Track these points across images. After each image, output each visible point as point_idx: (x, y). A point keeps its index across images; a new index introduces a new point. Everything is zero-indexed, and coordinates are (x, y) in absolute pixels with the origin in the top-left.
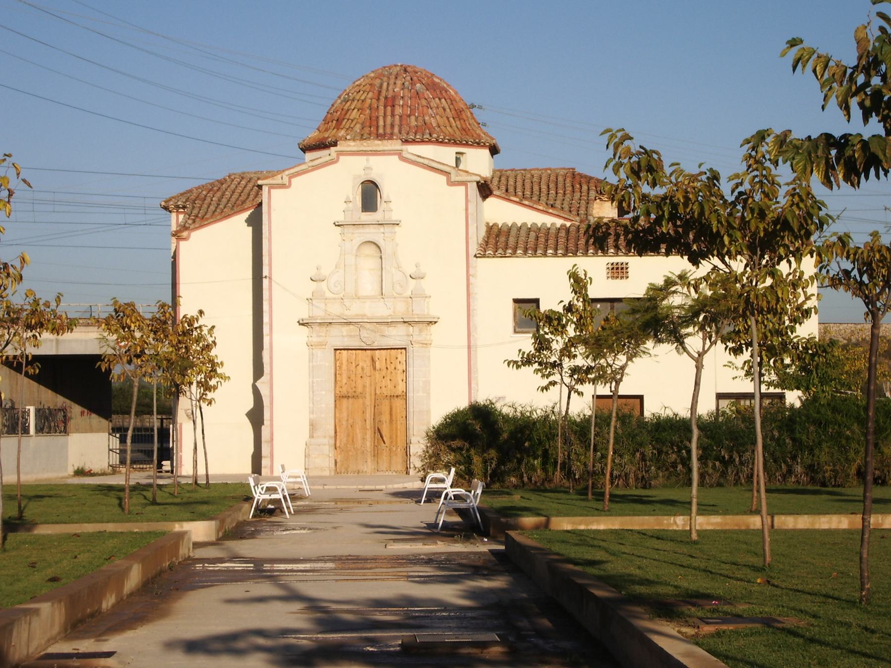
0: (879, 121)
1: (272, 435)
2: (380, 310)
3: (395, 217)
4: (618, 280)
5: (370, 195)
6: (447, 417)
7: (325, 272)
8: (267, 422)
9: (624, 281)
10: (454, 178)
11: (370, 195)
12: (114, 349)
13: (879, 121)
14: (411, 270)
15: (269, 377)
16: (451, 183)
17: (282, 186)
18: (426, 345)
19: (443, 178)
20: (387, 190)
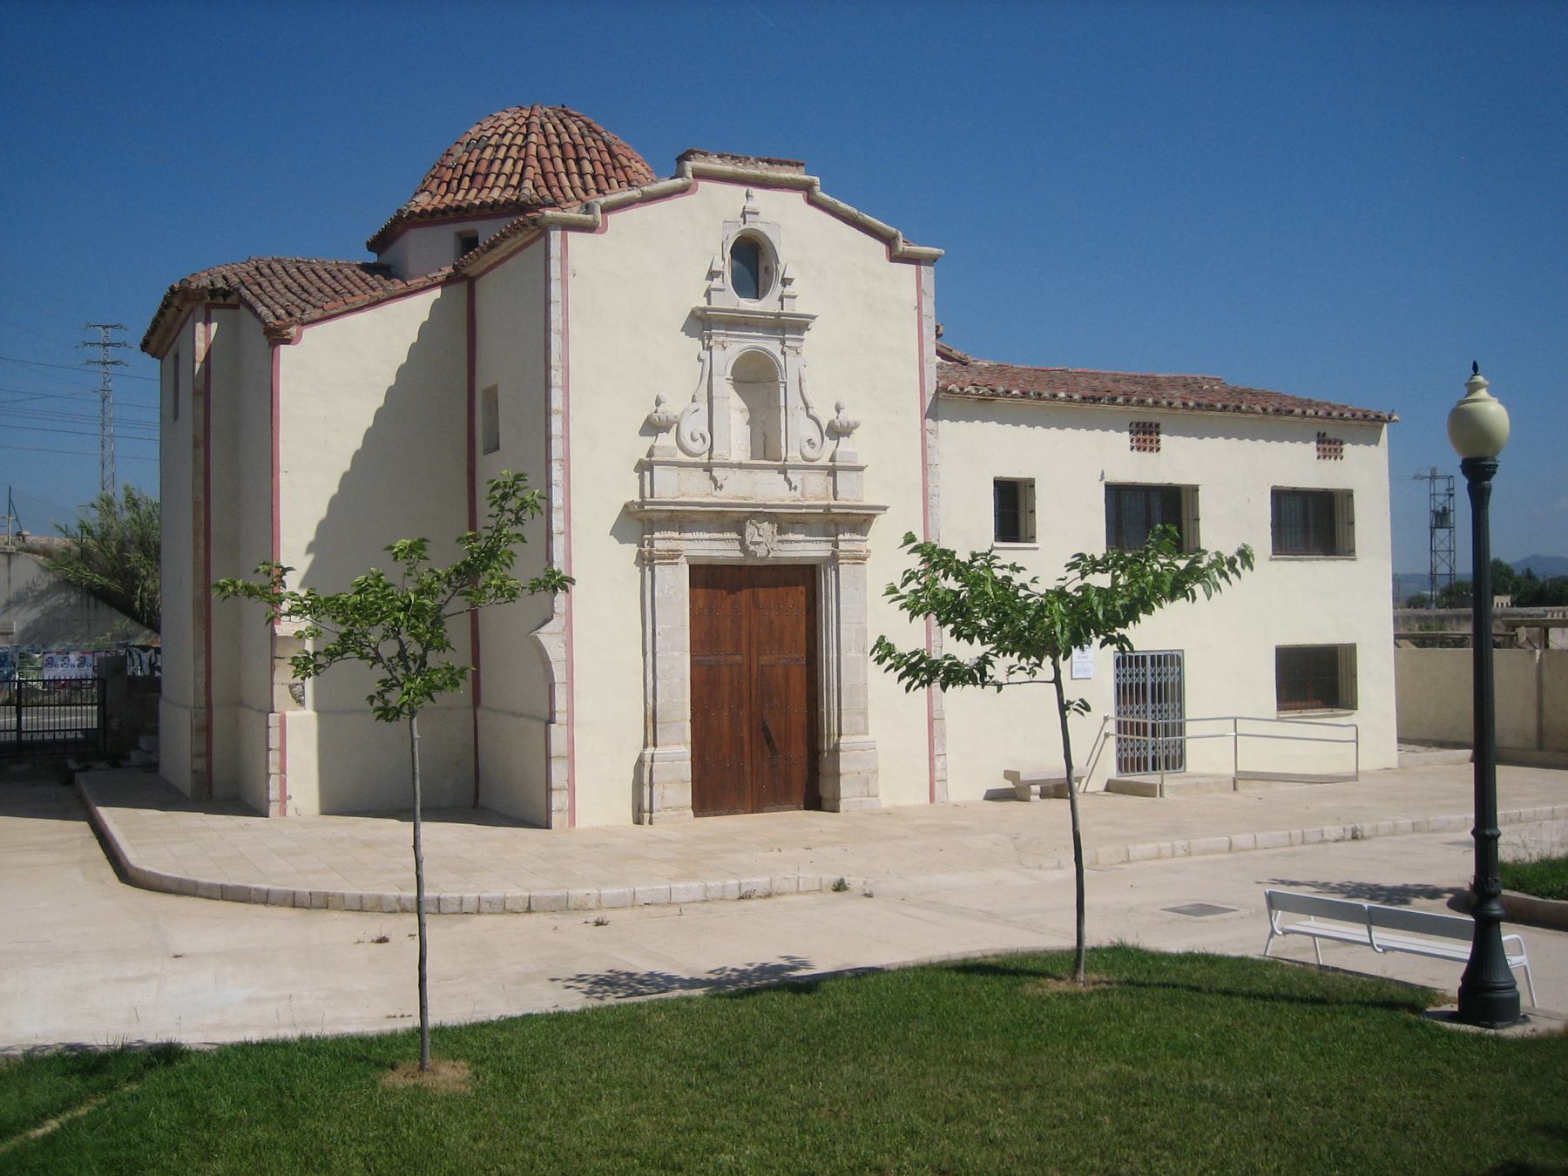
0: (1161, 606)
1: (571, 742)
2: (769, 489)
3: (797, 307)
4: (1147, 454)
5: (752, 260)
6: (71, 1047)
7: (671, 409)
8: (560, 717)
9: (1154, 455)
10: (901, 246)
11: (752, 260)
12: (476, 560)
13: (1161, 606)
14: (826, 416)
15: (563, 621)
16: (895, 257)
17: (589, 228)
18: (859, 559)
19: (880, 248)
20: (788, 256)
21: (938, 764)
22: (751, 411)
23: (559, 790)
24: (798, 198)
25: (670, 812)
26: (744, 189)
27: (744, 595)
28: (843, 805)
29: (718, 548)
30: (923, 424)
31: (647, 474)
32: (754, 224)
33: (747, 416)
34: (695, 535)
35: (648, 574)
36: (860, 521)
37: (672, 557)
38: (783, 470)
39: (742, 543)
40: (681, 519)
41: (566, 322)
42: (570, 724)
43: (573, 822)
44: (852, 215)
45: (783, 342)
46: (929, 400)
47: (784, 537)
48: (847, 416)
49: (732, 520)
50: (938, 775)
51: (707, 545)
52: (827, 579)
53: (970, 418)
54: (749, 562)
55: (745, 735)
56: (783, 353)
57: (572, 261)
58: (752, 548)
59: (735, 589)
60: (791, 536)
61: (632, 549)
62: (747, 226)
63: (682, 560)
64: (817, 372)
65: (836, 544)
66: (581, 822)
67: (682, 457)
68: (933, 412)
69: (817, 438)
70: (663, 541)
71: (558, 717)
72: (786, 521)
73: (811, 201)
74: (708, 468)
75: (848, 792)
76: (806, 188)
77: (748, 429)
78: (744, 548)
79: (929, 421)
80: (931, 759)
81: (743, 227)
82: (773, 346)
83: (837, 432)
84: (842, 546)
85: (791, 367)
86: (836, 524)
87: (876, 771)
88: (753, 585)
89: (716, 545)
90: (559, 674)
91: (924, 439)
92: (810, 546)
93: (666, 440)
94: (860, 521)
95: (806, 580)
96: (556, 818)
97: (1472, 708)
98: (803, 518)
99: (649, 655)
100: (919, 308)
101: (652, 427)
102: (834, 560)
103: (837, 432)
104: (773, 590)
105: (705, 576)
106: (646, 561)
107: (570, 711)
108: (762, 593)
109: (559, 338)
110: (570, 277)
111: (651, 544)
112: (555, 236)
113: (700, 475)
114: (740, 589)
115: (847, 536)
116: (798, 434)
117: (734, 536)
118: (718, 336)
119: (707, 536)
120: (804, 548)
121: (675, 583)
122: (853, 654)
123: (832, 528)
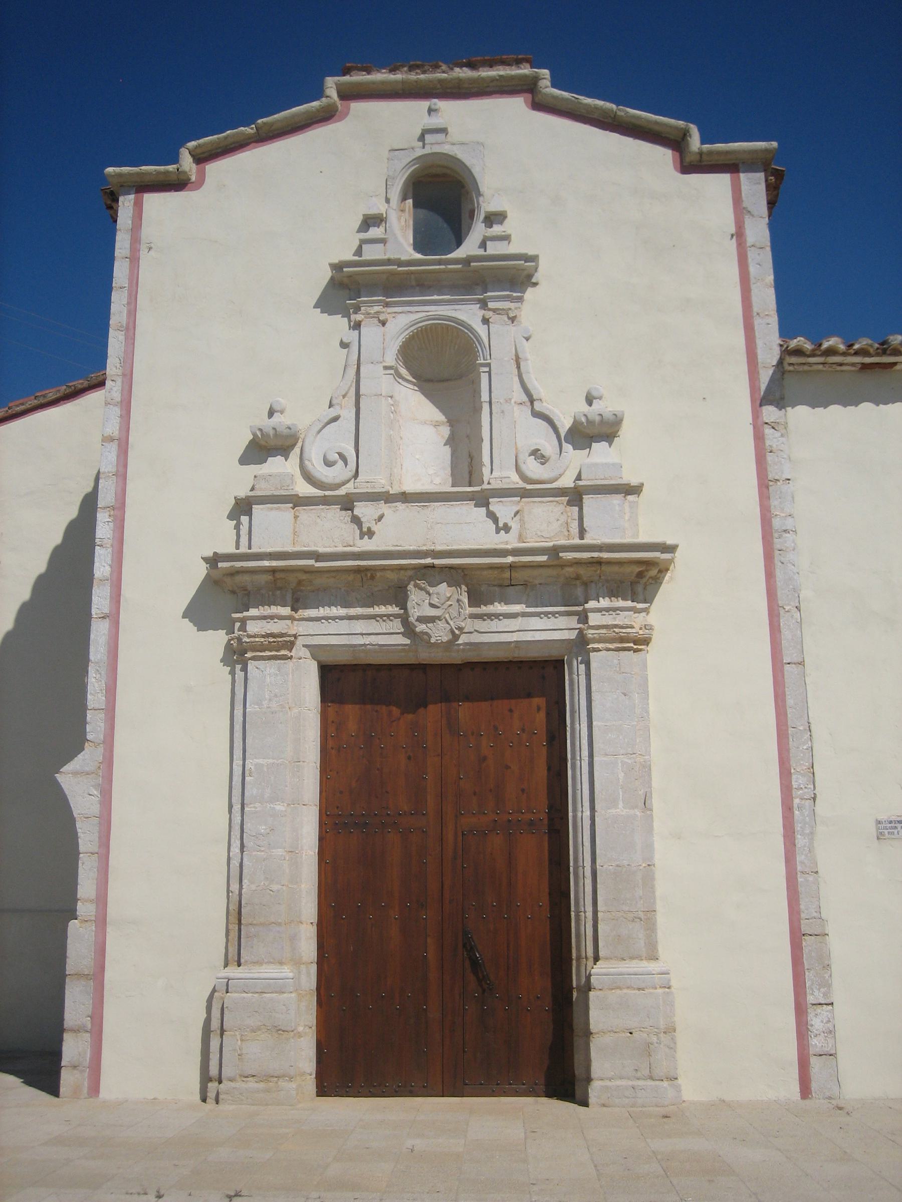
2: (464, 530)
5: (442, 196)
8: (84, 909)
10: (695, 142)
11: (442, 196)
16: (689, 166)
19: (664, 155)
20: (493, 189)
21: (816, 1021)
22: (452, 422)
23: (76, 1031)
24: (517, 104)
25: (252, 1084)
26: (424, 104)
27: (433, 713)
28: (595, 1091)
29: (366, 632)
30: (756, 415)
31: (244, 519)
32: (437, 146)
33: (446, 431)
34: (322, 612)
35: (240, 675)
36: (637, 575)
37: (279, 646)
38: (482, 500)
39: (405, 622)
40: (295, 584)
41: (132, 313)
42: (101, 921)
43: (95, 1088)
44: (605, 112)
45: (484, 304)
46: (765, 377)
47: (484, 609)
48: (605, 407)
49: (376, 582)
50: (816, 1043)
51: (344, 627)
52: (575, 675)
53: (850, 399)
54: (425, 656)
55: (431, 954)
56: (486, 321)
57: (148, 231)
58: (421, 628)
59: (417, 703)
60: (499, 608)
61: (216, 640)
62: (427, 150)
63: (299, 651)
64: (549, 350)
65: (583, 618)
66: (110, 1088)
67: (304, 489)
68: (777, 392)
69: (549, 446)
70: (261, 621)
71: (81, 908)
72: (485, 581)
73: (540, 105)
74: (347, 504)
75: (606, 1064)
76: (527, 88)
77: (447, 450)
78: (409, 630)
79: (770, 413)
80: (801, 1010)
81: (419, 152)
82: (468, 314)
83: (589, 433)
84: (594, 619)
85: (498, 340)
86: (586, 584)
87: (670, 1030)
88: (446, 698)
89: (360, 626)
90: (87, 838)
91: (759, 438)
92: (536, 623)
93: (280, 469)
94: (637, 575)
95: (539, 682)
96: (67, 1078)
97: (103, 1051)
98: (519, 576)
99: (237, 807)
100: (739, 235)
101: (261, 449)
102: (581, 645)
103: (589, 433)
104: (485, 705)
105: (345, 682)
106: (237, 655)
107: (102, 900)
108: (464, 711)
109: (121, 336)
110: (143, 254)
111: (243, 628)
112: (126, 204)
113: (334, 516)
114: (423, 704)
115: (604, 603)
116: (513, 440)
117: (393, 609)
118: (372, 306)
119: (342, 612)
120: (524, 627)
121: (293, 693)
122: (621, 810)
123: (579, 591)
